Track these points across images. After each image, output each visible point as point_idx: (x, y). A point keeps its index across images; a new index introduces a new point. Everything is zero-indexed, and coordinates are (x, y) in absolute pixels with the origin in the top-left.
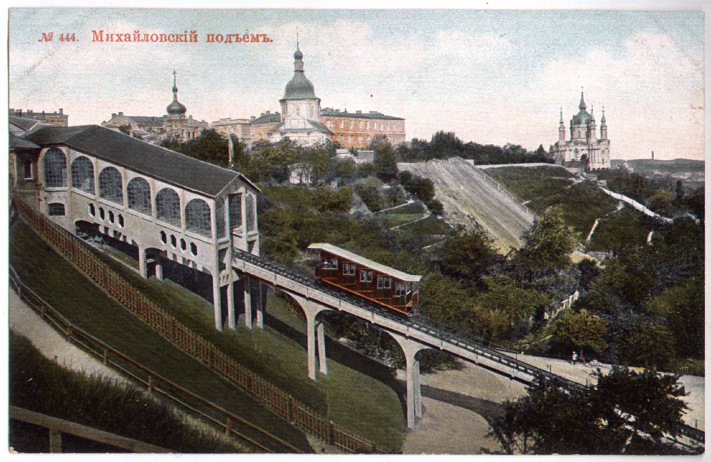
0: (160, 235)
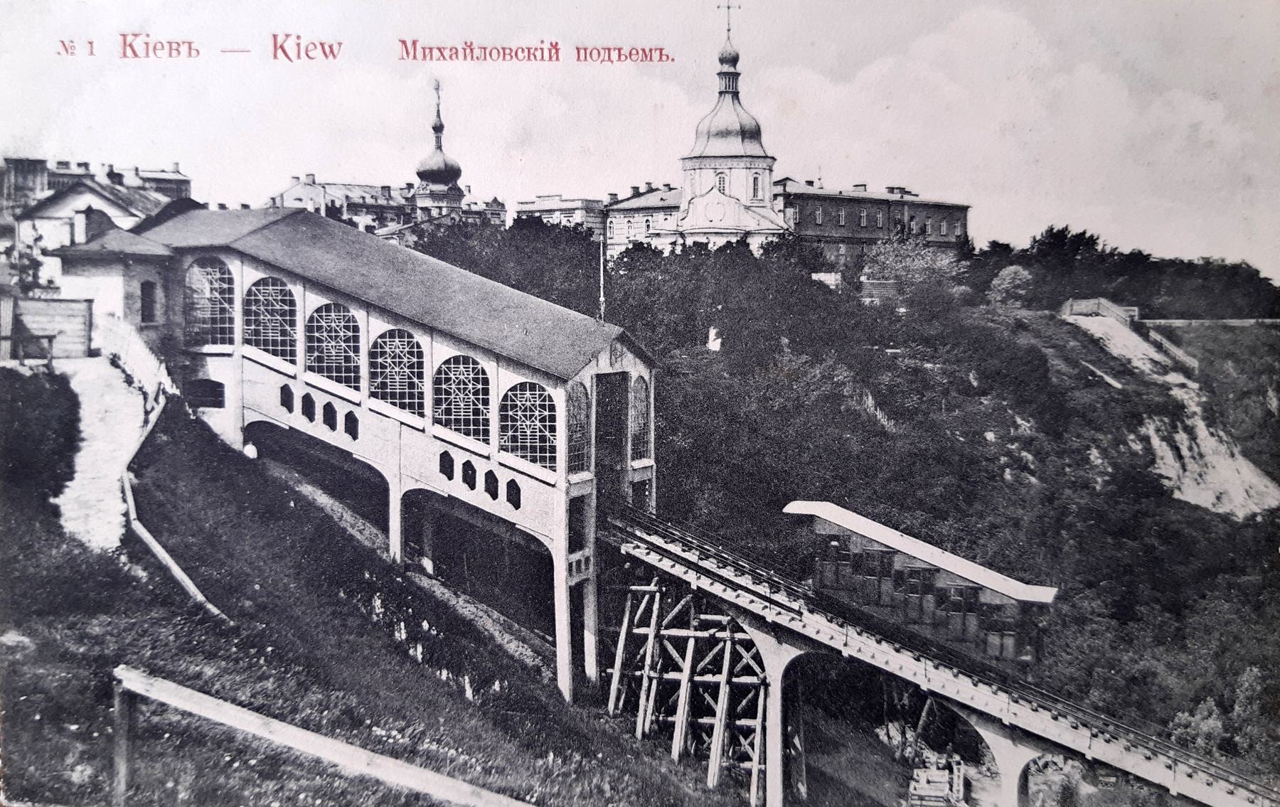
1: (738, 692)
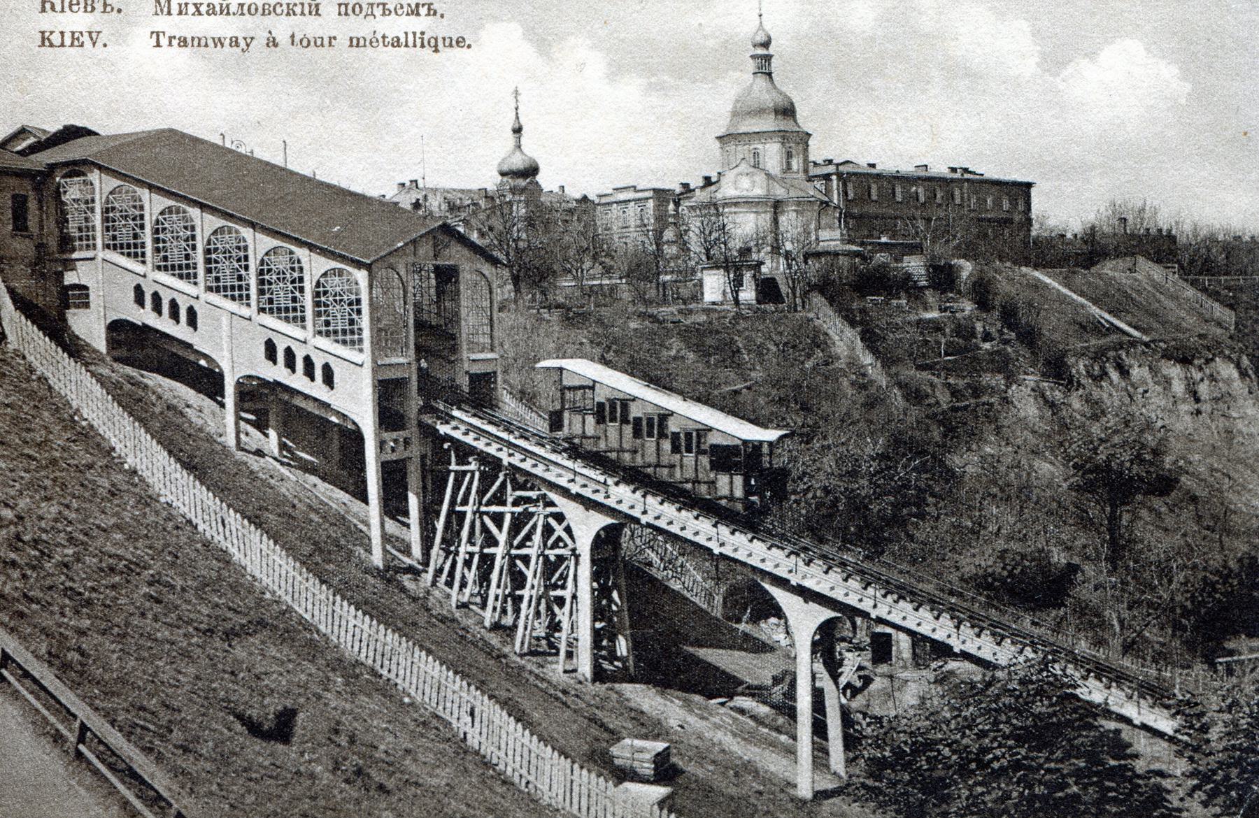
0: (132, 295)
1: (550, 567)
